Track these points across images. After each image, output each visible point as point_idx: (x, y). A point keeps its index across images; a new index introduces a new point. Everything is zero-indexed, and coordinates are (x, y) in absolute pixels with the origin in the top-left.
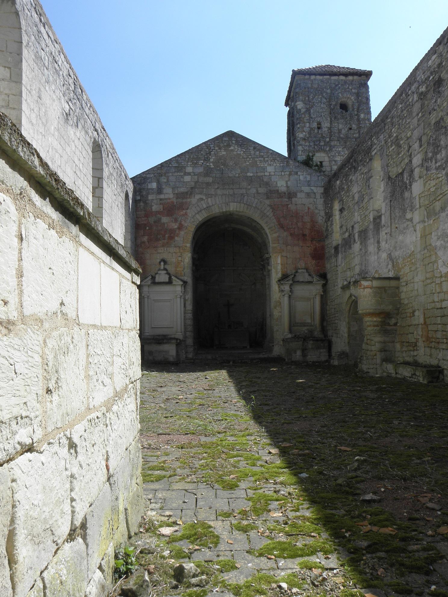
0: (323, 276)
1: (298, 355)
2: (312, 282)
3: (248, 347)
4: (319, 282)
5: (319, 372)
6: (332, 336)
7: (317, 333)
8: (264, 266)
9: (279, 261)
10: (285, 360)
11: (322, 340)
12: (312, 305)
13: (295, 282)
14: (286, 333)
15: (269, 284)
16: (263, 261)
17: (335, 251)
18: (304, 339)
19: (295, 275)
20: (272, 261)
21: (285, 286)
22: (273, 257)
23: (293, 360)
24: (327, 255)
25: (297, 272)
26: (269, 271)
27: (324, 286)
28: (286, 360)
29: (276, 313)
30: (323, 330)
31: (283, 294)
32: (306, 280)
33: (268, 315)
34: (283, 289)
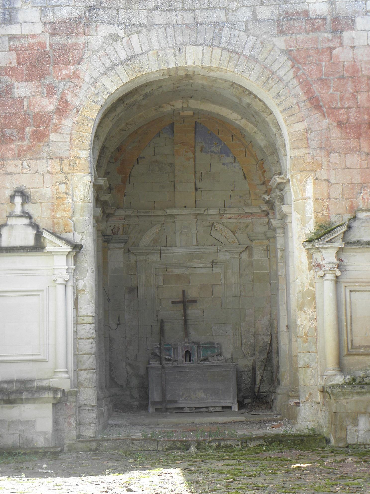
3: (235, 408)
8: (271, 205)
9: (310, 191)
10: (328, 442)
13: (349, 243)
14: (329, 373)
15: (285, 250)
19: (349, 227)
20: (293, 192)
21: (325, 255)
23: (349, 442)
25: (354, 218)
26: (284, 217)
28: (333, 442)
29: (303, 322)
31: (321, 273)
33: (283, 327)
34: (319, 261)
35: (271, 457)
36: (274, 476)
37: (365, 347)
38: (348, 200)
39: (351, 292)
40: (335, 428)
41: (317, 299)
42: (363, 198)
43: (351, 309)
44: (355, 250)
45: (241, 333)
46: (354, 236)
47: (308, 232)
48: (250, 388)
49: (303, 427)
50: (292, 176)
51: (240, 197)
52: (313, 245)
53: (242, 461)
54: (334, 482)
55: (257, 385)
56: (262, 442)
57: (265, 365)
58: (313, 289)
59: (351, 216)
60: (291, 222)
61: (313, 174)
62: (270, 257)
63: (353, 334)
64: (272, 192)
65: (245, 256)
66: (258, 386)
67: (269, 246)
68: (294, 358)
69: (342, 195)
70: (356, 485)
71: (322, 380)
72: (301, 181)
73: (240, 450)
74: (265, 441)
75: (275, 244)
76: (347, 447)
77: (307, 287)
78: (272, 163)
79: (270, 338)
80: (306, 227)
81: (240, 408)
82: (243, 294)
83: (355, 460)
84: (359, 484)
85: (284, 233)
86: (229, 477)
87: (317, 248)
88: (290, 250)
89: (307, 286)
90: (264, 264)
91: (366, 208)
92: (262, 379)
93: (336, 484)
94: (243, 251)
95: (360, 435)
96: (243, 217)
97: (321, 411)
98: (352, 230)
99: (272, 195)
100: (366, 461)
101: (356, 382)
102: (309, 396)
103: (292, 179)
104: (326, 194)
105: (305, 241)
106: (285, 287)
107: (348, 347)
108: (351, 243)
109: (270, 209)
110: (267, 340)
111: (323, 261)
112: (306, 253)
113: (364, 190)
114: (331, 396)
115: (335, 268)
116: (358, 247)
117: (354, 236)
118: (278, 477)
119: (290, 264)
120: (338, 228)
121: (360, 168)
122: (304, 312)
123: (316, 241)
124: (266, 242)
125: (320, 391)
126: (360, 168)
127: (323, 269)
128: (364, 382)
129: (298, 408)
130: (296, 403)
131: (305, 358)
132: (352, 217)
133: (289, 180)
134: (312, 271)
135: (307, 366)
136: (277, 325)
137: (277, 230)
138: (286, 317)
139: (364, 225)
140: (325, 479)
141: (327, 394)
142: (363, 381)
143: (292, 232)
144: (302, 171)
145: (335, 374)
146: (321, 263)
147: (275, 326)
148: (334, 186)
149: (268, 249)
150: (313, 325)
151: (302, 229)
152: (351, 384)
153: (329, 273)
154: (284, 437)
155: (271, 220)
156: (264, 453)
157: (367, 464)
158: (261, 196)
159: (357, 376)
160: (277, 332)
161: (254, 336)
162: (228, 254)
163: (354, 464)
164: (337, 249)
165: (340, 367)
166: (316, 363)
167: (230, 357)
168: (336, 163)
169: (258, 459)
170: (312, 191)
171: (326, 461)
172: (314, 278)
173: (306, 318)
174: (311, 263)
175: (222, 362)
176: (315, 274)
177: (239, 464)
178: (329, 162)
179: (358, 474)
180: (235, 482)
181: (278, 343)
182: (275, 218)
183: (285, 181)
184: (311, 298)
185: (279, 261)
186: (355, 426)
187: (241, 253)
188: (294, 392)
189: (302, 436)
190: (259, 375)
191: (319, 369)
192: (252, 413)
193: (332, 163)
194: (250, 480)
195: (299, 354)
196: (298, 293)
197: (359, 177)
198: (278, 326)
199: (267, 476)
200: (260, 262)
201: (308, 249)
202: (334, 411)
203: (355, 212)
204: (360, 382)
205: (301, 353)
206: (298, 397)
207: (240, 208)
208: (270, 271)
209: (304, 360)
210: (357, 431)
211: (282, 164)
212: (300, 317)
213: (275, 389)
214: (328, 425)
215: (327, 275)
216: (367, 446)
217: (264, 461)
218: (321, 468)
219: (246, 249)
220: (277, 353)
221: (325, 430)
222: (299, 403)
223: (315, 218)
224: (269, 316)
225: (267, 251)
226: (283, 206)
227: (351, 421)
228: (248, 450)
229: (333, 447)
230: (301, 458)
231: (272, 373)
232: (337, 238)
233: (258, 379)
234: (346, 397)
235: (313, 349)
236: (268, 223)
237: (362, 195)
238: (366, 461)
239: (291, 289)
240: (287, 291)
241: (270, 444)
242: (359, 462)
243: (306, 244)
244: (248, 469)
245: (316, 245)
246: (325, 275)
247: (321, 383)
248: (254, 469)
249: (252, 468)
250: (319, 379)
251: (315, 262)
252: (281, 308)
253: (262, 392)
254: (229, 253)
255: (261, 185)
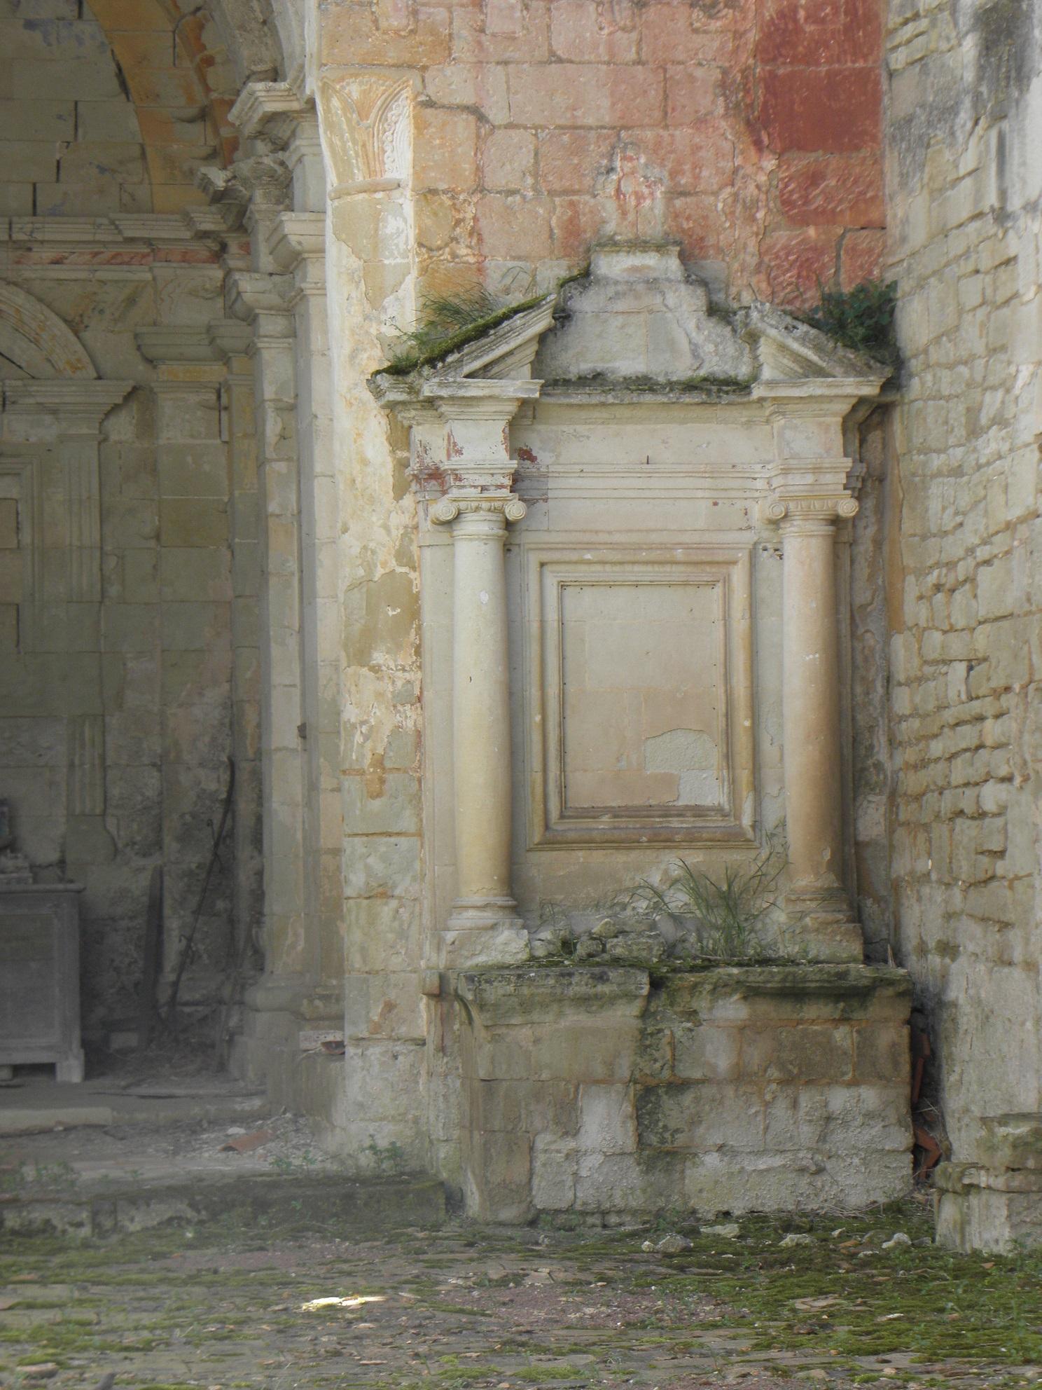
0: (863, 325)
1: (593, 1151)
2: (740, 387)
3: (72, 1070)
4: (815, 387)
5: (820, 1327)
6: (949, 949)
7: (795, 920)
8: (236, 211)
9: (399, 160)
10: (454, 1201)
11: (847, 995)
12: (740, 625)
13: (563, 385)
14: (470, 918)
15: (295, 407)
16: (224, 153)
17: (987, 47)
18: (657, 984)
19: (563, 316)
20: (328, 156)
21: (462, 431)
22: (330, 109)
23: (542, 1199)
24: (902, 98)
25: (584, 278)
26: (293, 263)
27: (869, 422)
28: (474, 1201)
29: (367, 709)
30: (856, 881)
31: (443, 508)
32: (683, 370)
33: (283, 733)
34: (438, 456)
35: (216, 1272)
36: (227, 1346)
37: (616, 813)
38: (557, 200)
39: (563, 586)
40: (486, 1147)
41: (429, 617)
42: (618, 190)
43: (563, 658)
44: (583, 414)
45: (103, 758)
46: (578, 356)
47: (390, 332)
48: (136, 985)
49: (355, 1146)
50: (325, 88)
51: (102, 170)
52: (412, 390)
53: (95, 1289)
54: (477, 1368)
55: (169, 976)
56: (182, 1208)
57: (204, 890)
58: (413, 575)
59: (569, 268)
60: (322, 289)
61: (413, 79)
62: (231, 434)
63: (568, 760)
64: (238, 154)
65: (123, 428)
66: (172, 977)
67: (229, 389)
68: (326, 860)
69: (535, 175)
70: (565, 1376)
71: (439, 949)
72: (362, 110)
73: (86, 1245)
74: (193, 1205)
75: (253, 380)
76: (533, 1223)
77: (384, 564)
78: (242, 27)
79: (226, 777)
80: (385, 309)
81: (91, 1070)
82: (114, 590)
83: (561, 1276)
84: (577, 1373)
85: (294, 335)
86: (39, 1354)
87: (431, 403)
88: (315, 408)
89: (385, 563)
90: (207, 467)
91: (631, 236)
92: (189, 947)
93: (483, 1375)
94: (115, 408)
95: (584, 1173)
96: (114, 260)
97: (430, 1074)
98: (573, 328)
99: (242, 165)
100: (609, 1281)
101: (575, 957)
102: (382, 1015)
103: (328, 101)
104: (467, 168)
105: (378, 372)
106: (293, 565)
107: (546, 812)
108: (567, 382)
109: (230, 230)
110: (213, 786)
111: (455, 458)
112: (384, 421)
113: (623, 159)
114: (474, 1013)
115: (502, 486)
116: (595, 399)
117: (578, 356)
118: (246, 1350)
119: (318, 468)
120: (518, 320)
121: (608, 63)
122: (376, 669)
123: (426, 370)
124: (215, 372)
125: (430, 995)
126: (608, 63)
127: (454, 493)
128: (606, 957)
129: (334, 1066)
130: (327, 1045)
131: (370, 860)
132: (575, 272)
133: (311, 104)
134: (408, 500)
135: (380, 892)
136: (259, 726)
137: (262, 320)
138: (297, 692)
139: (621, 306)
140: (440, 1354)
141: (457, 1006)
142: (604, 951)
143: (325, 332)
144: (369, 64)
145: (493, 921)
146: (446, 466)
147: (250, 730)
148: (499, 134)
149: (224, 401)
150: (410, 724)
151: (366, 318)
152: (557, 964)
153: (477, 509)
154: (274, 1185)
155: (237, 276)
156: (190, 1253)
157: (609, 1292)
158: (192, 172)
159: (580, 928)
160: (258, 754)
161: (160, 771)
162: (48, 419)
163: (559, 1291)
164: (512, 408)
165: (512, 894)
166: (414, 879)
167: (54, 856)
168: (511, 38)
169: (162, 1281)
170: (409, 155)
171: (445, 1282)
172: (416, 527)
173: (380, 695)
174: (403, 464)
175: (19, 880)
176: (421, 513)
177: (81, 1302)
178: (482, 31)
179: (576, 1333)
180: (64, 1375)
181: (260, 799)
182: (252, 269)
183: (296, 106)
184: (401, 611)
185: (270, 453)
186: (566, 1133)
187: (107, 415)
188: (321, 999)
189: (348, 1179)
190: (175, 933)
191: (427, 904)
192: (143, 1090)
193: (494, 35)
194: (127, 1366)
195: (347, 843)
196: (351, 589)
197: (606, 103)
198: (262, 727)
199: (197, 1346)
200: (189, 459)
201: (392, 407)
202: (482, 1074)
203: (588, 250)
204: (590, 955)
205: (357, 839)
206: (338, 1020)
207: (99, 220)
208: (232, 494)
209: (367, 866)
210: (574, 1156)
211: (282, 34)
212: (353, 689)
213: (243, 987)
214: (456, 1133)
215: (470, 517)
216: (613, 1219)
217: (188, 1288)
218: (423, 1310)
219: (128, 397)
220: (257, 841)
221: (443, 1152)
222: (340, 1045)
223: (424, 271)
224: (226, 686)
225: (221, 408)
226: (286, 216)
227: (550, 1115)
228: (122, 1242)
229: (474, 1222)
230: (342, 1273)
231: (232, 922)
232: (509, 361)
233: (173, 947)
234: (535, 1016)
235: (407, 822)
236: (223, 287)
237: (614, 177)
238: (609, 1281)
239: (320, 572)
240: (301, 580)
241: (214, 1216)
242: (579, 1283)
243: (385, 381)
244: (119, 1319)
245: (427, 390)
246: (459, 515)
247: (433, 959)
248: (147, 1319)
249: (135, 1316)
250: (427, 948)
251: (421, 462)
252: (275, 651)
253: (187, 1004)
254: (54, 412)
255: (191, 121)
